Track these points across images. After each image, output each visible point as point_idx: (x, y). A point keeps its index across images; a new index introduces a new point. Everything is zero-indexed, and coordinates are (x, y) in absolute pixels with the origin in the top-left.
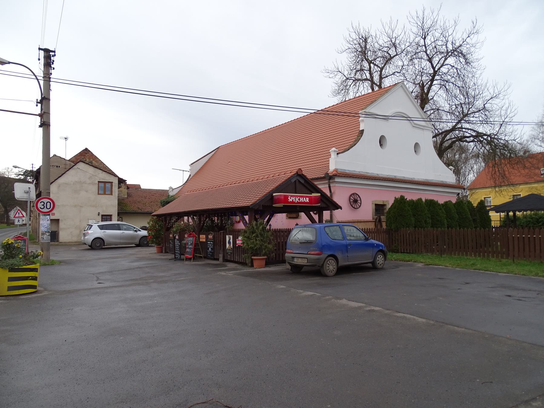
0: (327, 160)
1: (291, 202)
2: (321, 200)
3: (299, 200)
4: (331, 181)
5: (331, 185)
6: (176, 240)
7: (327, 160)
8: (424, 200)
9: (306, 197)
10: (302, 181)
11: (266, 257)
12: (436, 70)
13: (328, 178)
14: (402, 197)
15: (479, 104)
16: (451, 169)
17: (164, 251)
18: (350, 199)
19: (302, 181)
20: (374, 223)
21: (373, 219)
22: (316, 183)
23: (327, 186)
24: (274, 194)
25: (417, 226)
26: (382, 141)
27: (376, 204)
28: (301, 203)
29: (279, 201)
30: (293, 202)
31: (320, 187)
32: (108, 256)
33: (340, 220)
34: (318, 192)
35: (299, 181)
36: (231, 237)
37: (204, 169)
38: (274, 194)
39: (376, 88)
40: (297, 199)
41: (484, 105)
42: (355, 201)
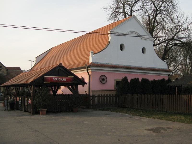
0: (88, 58)
1: (54, 81)
2: (74, 79)
3: (60, 79)
4: (88, 69)
5: (89, 71)
6: (6, 100)
7: (88, 58)
8: (129, 80)
9: (64, 78)
10: (63, 70)
11: (46, 109)
12: (157, 8)
13: (86, 67)
14: (125, 79)
15: (185, 26)
16: (165, 62)
17: (70, 110)
18: (100, 78)
19: (63, 70)
20: (115, 91)
21: (115, 89)
22: (71, 71)
23: (86, 71)
24: (44, 77)
25: (135, 94)
26: (122, 47)
27: (117, 81)
28: (61, 81)
29: (47, 80)
30: (56, 81)
31: (74, 73)
32: (174, 98)
33: (94, 89)
34: (73, 76)
35: (61, 69)
36: (27, 98)
37: (41, 59)
38: (44, 77)
39: (127, 17)
40: (59, 79)
41: (188, 27)
42: (103, 79)
